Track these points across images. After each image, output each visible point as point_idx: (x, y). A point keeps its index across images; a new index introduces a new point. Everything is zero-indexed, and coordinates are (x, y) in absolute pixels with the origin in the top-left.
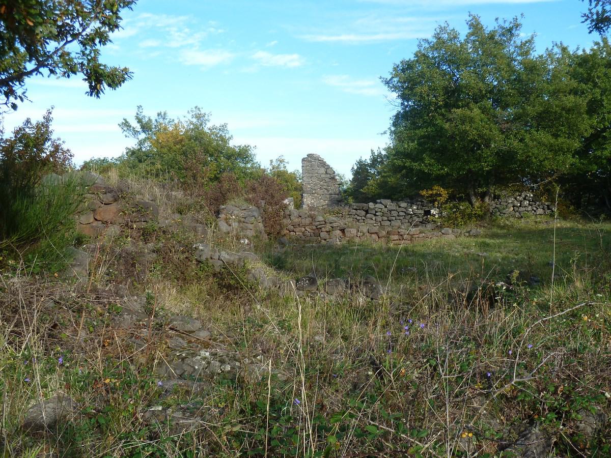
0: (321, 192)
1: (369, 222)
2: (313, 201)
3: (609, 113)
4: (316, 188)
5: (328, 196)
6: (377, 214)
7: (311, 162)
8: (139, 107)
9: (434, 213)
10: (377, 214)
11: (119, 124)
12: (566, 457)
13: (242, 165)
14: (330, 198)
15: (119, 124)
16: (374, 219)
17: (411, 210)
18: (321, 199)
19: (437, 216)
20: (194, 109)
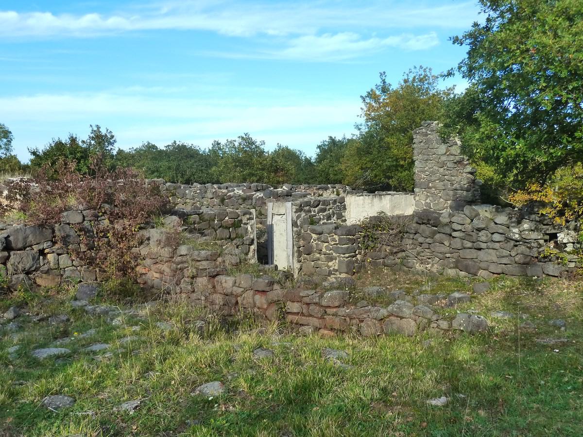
0: (439, 185)
1: (437, 249)
2: (428, 201)
3: (581, 61)
4: (433, 178)
5: (451, 193)
6: (454, 234)
7: (426, 135)
8: (383, 74)
9: (565, 241)
10: (454, 234)
11: (361, 97)
12: (64, 433)
13: (510, 115)
14: (454, 195)
15: (361, 97)
16: (446, 243)
17: (516, 230)
18: (441, 197)
19: (570, 248)
20: (418, 67)
